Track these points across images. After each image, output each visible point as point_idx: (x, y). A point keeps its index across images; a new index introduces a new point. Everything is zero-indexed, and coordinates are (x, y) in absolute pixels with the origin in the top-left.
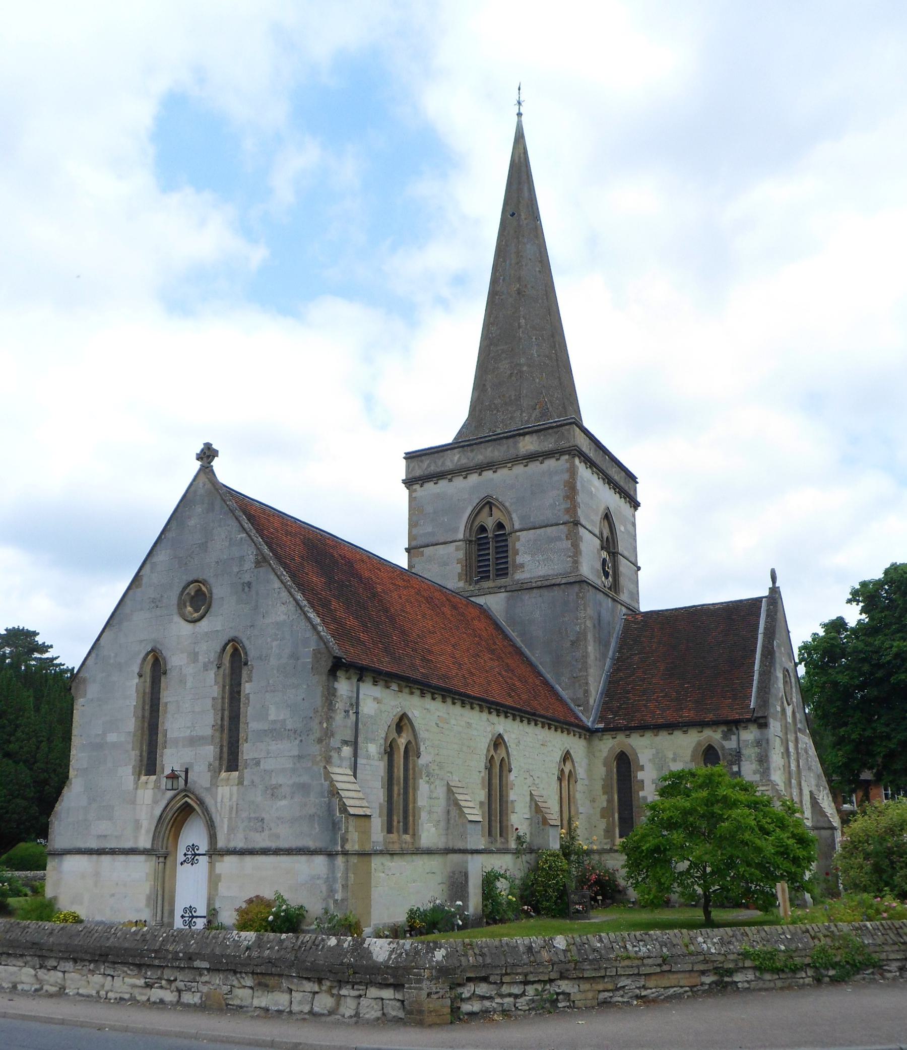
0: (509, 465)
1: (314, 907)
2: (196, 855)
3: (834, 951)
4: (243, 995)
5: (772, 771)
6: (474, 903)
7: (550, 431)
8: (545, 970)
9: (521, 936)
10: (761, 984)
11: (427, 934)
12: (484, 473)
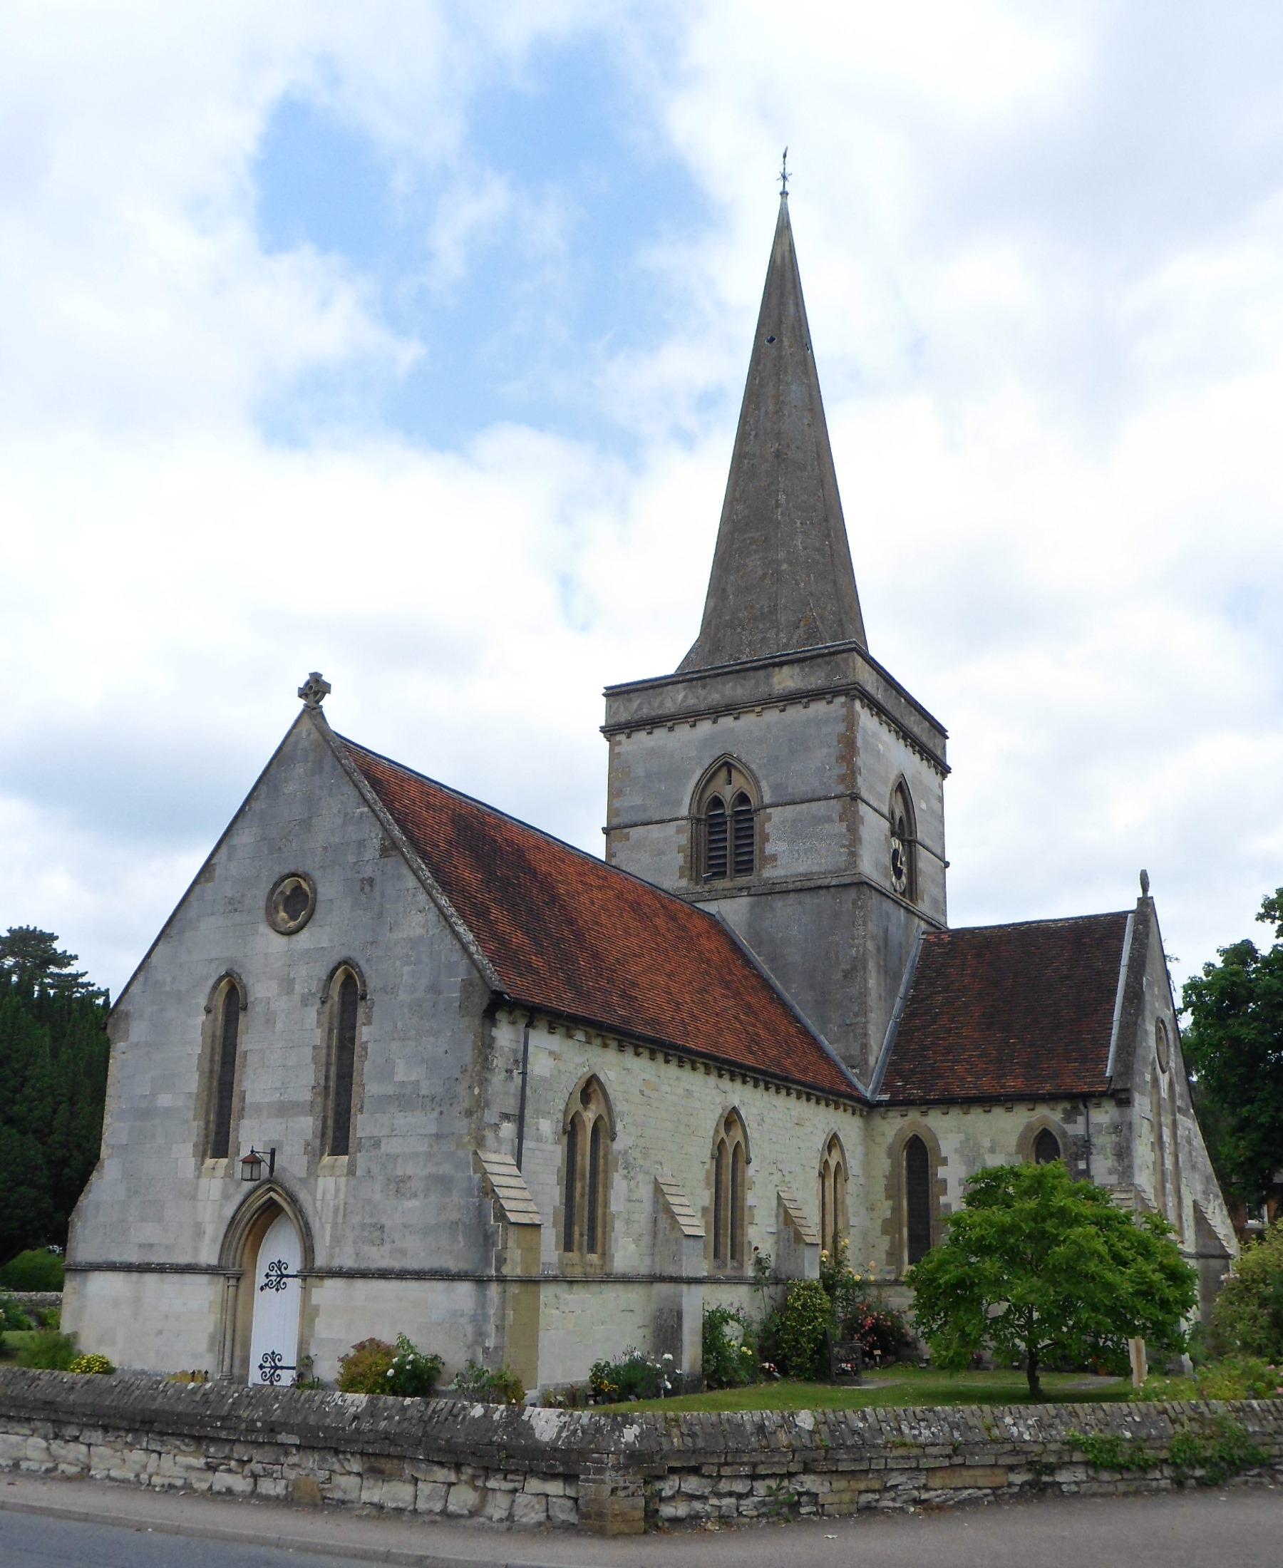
0: (758, 709)
1: (455, 1357)
2: (282, 1276)
3: (1203, 1442)
5: (1136, 1171)
6: (690, 1356)
7: (820, 660)
8: (783, 1460)
9: (749, 1410)
10: (1095, 1487)
11: (619, 1401)
12: (721, 720)
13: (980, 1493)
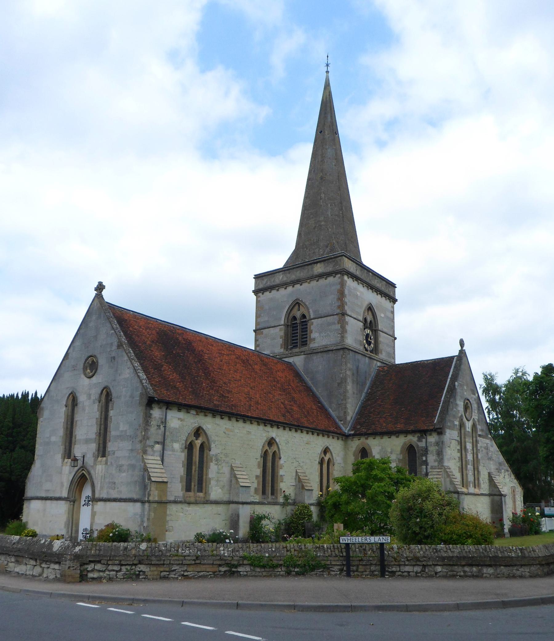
0: (308, 281)
4: (12, 566)
6: (244, 530)
8: (131, 559)
10: (254, 573)
12: (296, 286)
13: (208, 574)
